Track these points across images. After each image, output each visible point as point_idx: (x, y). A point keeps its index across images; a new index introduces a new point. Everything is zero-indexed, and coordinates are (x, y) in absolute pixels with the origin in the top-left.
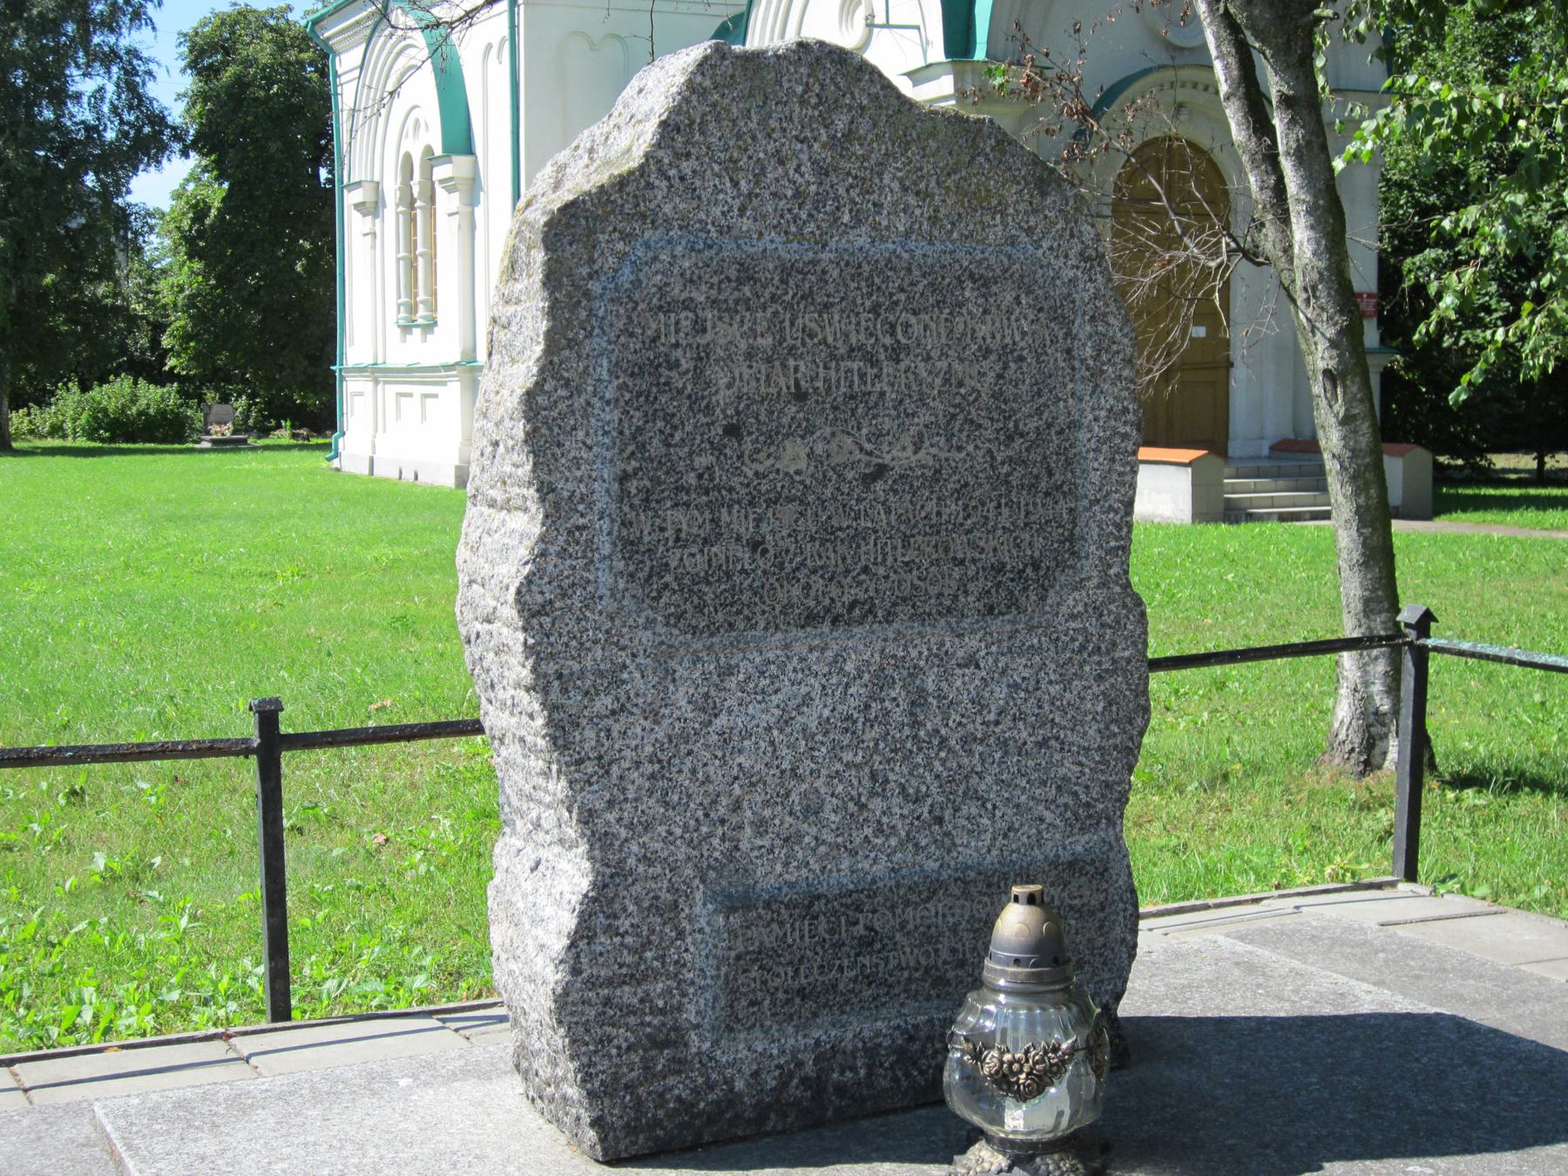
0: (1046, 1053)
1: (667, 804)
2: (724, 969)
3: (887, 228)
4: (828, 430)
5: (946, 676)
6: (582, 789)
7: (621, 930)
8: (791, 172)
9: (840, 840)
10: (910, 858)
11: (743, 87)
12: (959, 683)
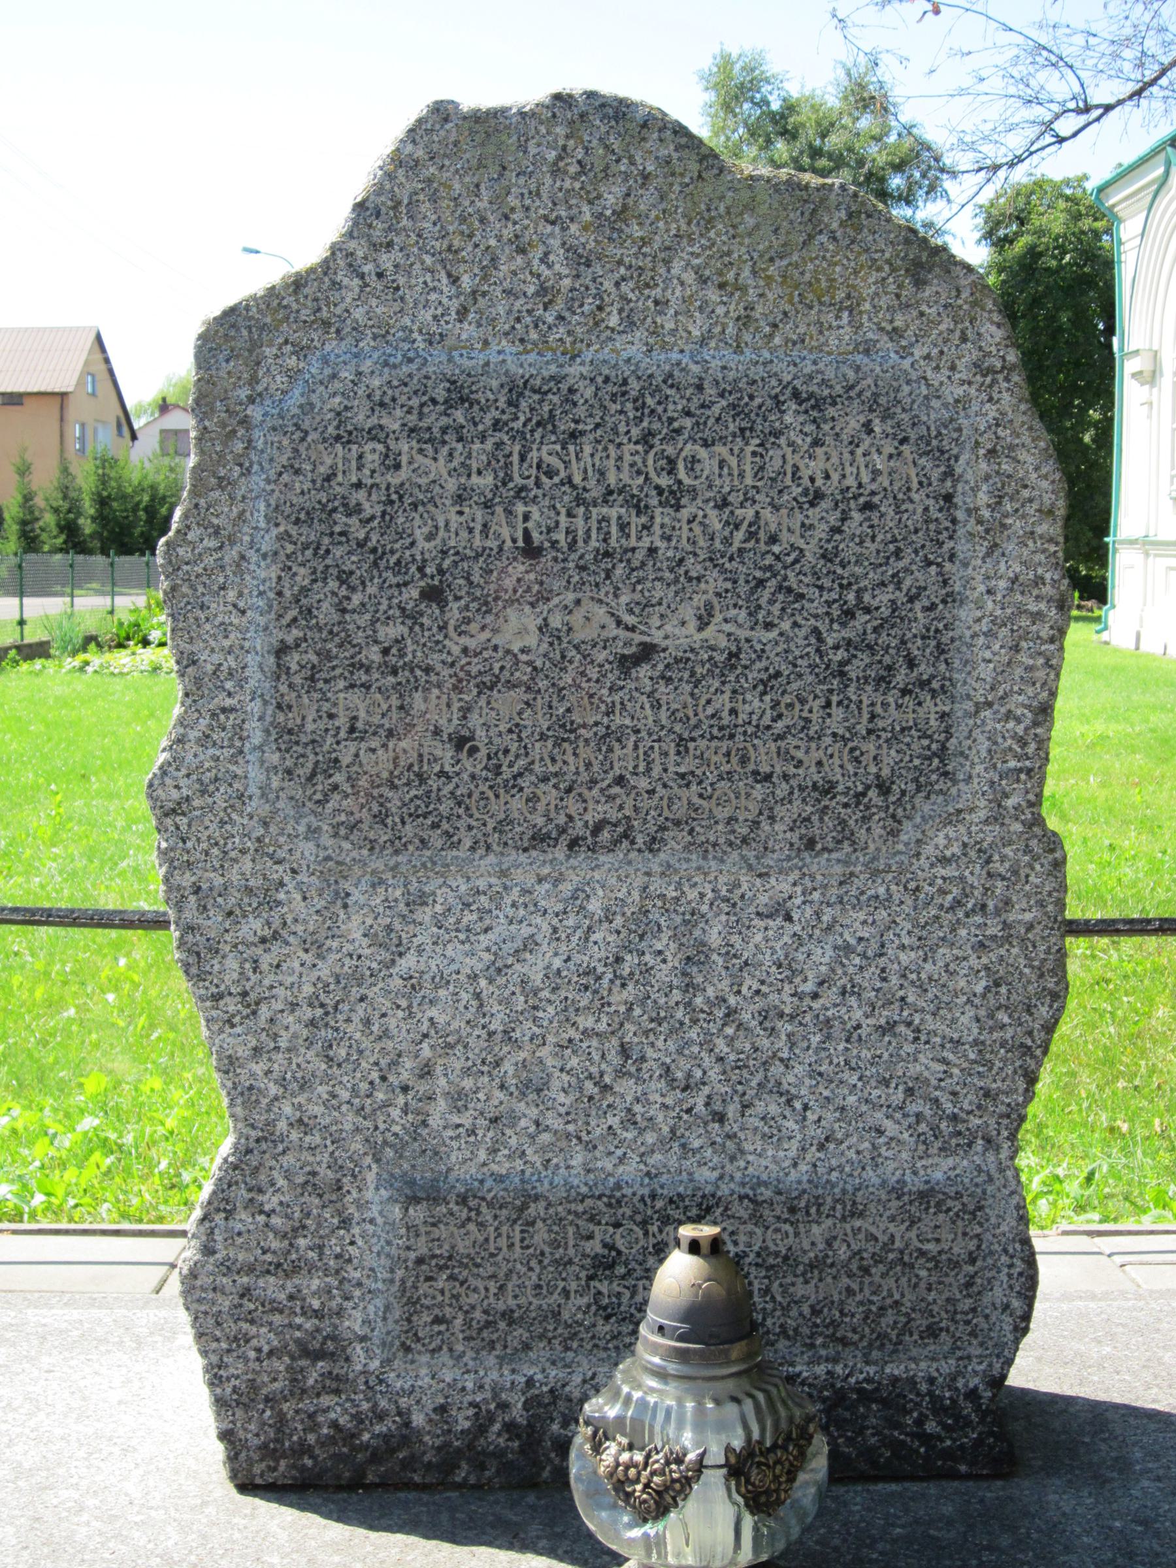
0: (668, 1463)
1: (330, 1059)
2: (400, 1273)
3: (673, 332)
4: (570, 597)
5: (740, 927)
6: (221, 1031)
7: (267, 1208)
8: (536, 262)
9: (571, 1128)
10: (673, 1163)
11: (470, 154)
12: (758, 938)
